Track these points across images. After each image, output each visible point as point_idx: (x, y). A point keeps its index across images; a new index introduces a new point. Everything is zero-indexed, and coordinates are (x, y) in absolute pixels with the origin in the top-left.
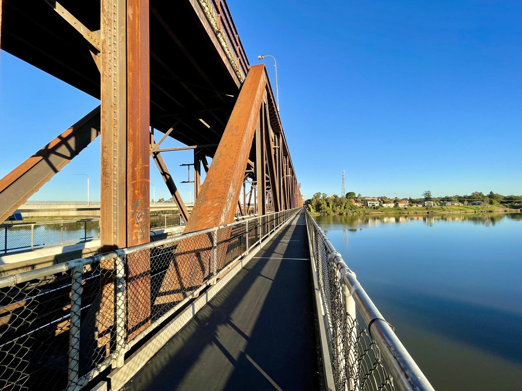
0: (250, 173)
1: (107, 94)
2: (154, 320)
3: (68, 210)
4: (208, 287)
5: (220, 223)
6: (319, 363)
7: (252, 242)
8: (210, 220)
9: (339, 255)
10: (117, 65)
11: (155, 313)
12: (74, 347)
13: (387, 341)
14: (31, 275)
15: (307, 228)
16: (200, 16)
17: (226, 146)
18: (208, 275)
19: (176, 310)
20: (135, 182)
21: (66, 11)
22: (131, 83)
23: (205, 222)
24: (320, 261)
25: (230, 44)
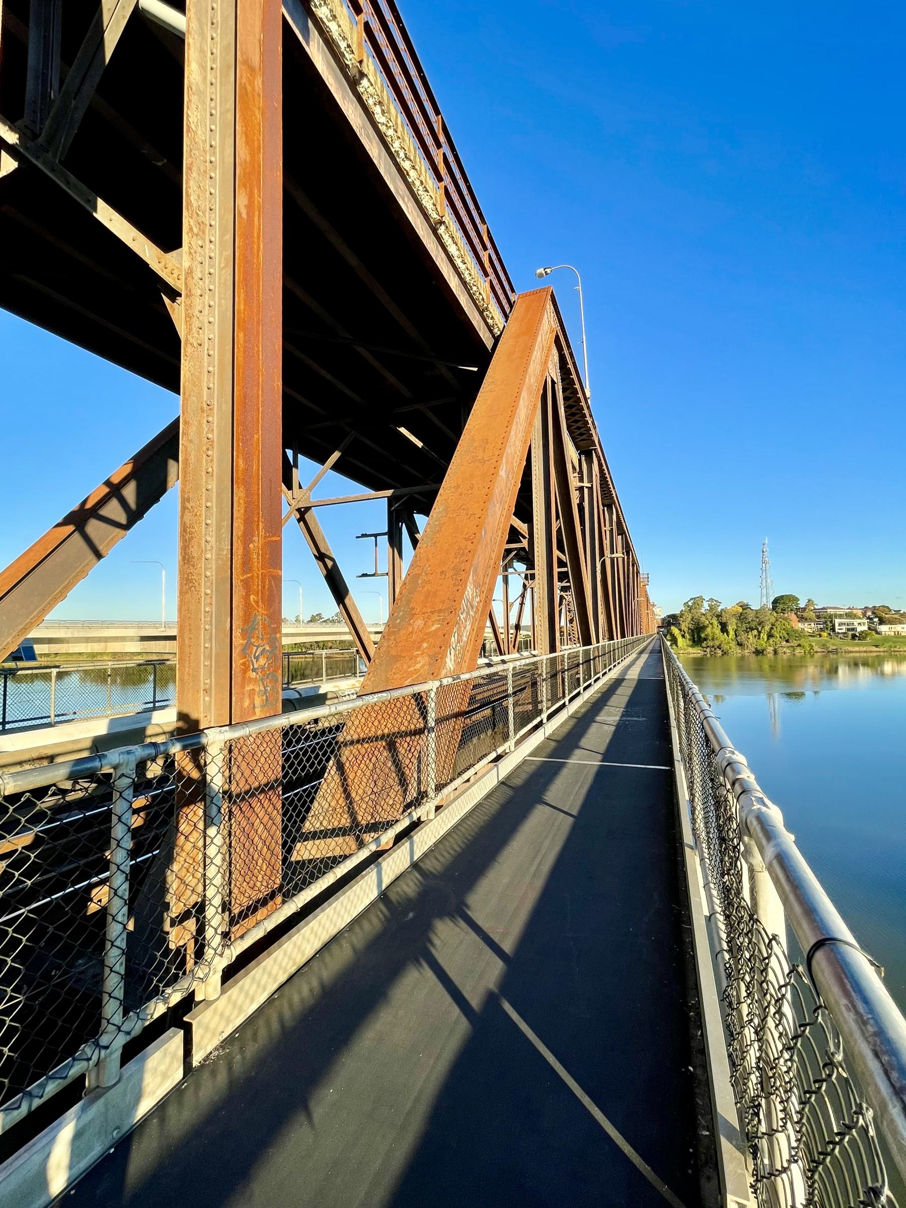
0: (519, 551)
1: (194, 384)
2: (288, 896)
3: (123, 639)
4: (415, 825)
5: (444, 672)
6: (694, 1044)
7: (523, 719)
8: (421, 664)
9: (740, 758)
10: (216, 320)
11: (291, 880)
12: (115, 944)
13: (857, 1006)
14: (32, 779)
15: (665, 688)
16: (398, 193)
17: (458, 487)
18: (415, 795)
19: (339, 876)
20: (249, 575)
21: (116, 216)
22: (241, 354)
23: (409, 668)
24: (696, 772)
25: (468, 247)
